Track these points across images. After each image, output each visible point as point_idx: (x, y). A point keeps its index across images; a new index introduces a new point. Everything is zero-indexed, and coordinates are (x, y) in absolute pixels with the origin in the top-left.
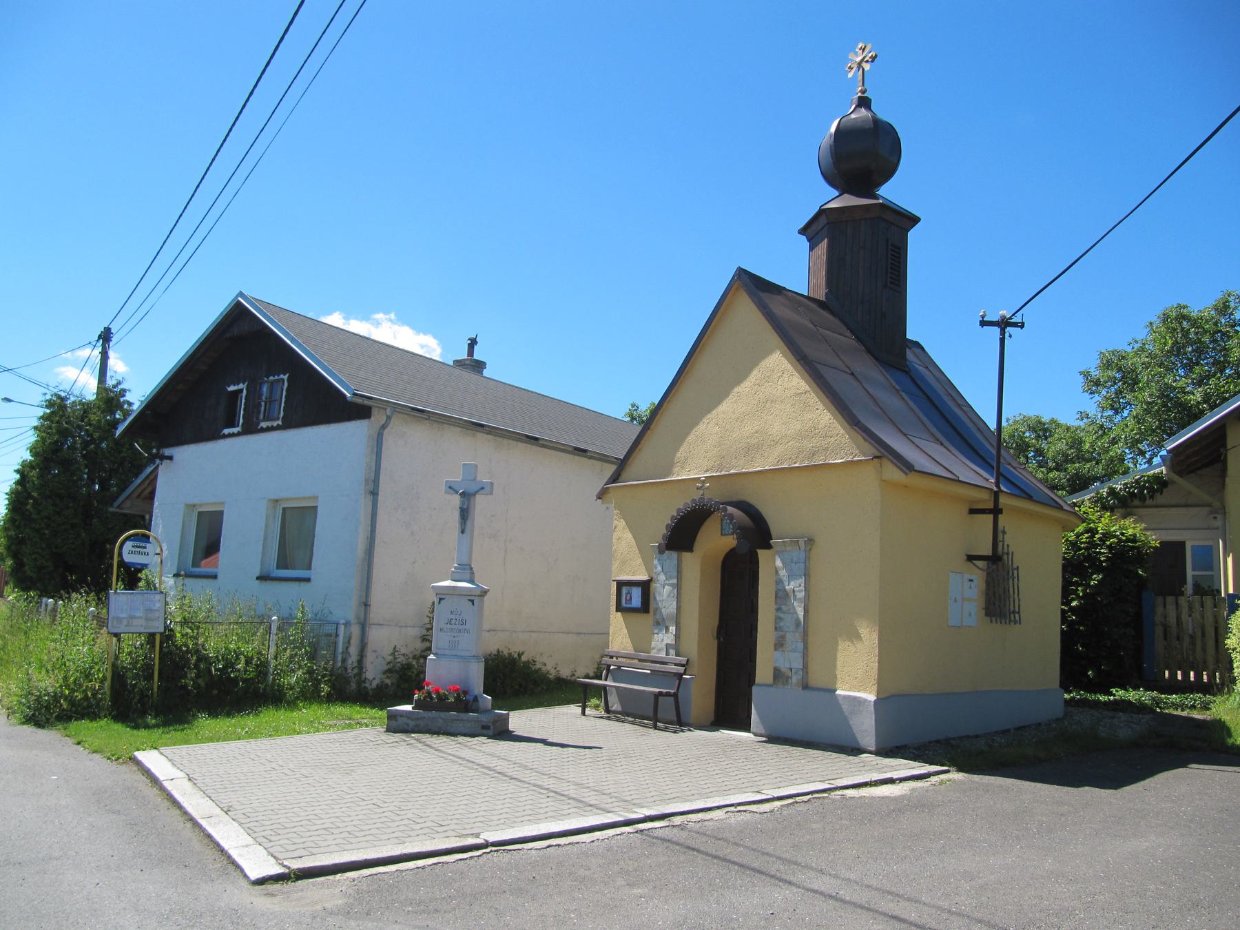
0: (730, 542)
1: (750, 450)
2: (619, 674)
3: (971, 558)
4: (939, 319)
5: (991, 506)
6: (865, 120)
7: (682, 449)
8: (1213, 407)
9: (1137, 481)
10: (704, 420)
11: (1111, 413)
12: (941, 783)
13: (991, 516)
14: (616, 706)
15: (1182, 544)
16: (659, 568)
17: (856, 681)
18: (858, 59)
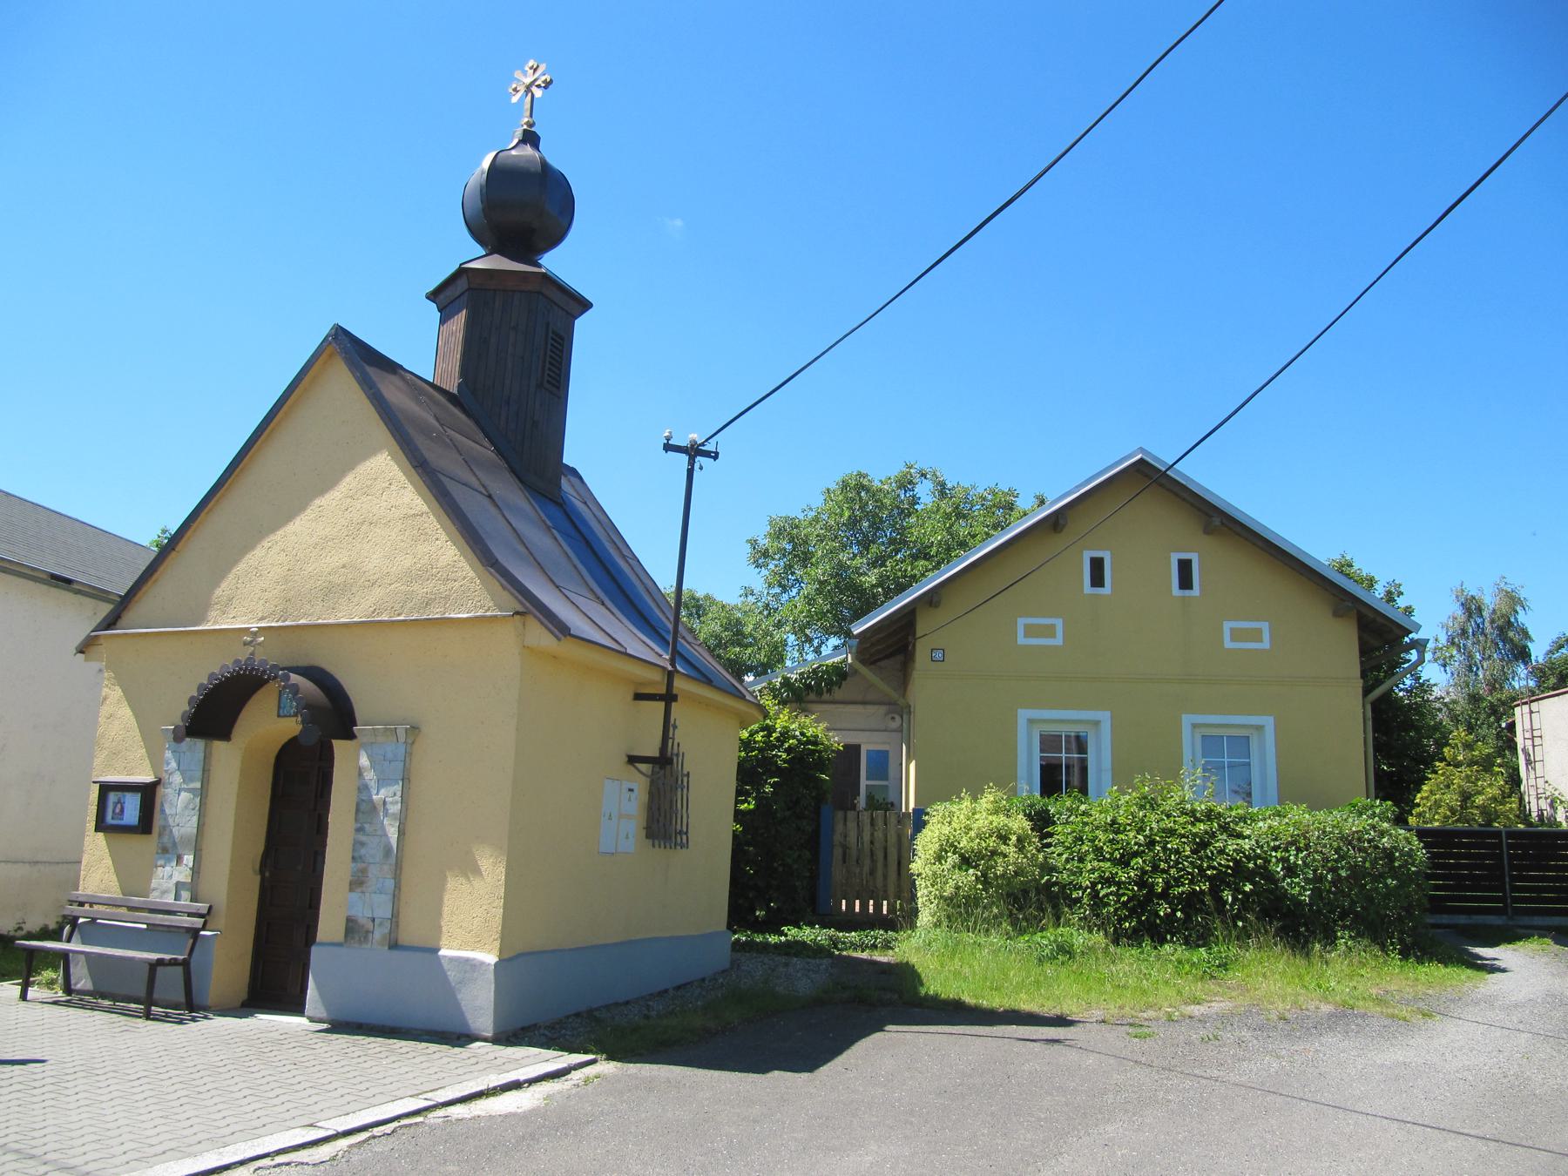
0: (292, 727)
1: (332, 592)
2: (94, 931)
3: (633, 760)
4: (609, 438)
5: (663, 690)
6: (529, 160)
7: (224, 585)
8: (889, 595)
9: (815, 671)
10: (266, 543)
11: (778, 590)
12: (587, 1081)
13: (661, 705)
14: (82, 981)
15: (857, 748)
16: (174, 765)
17: (470, 935)
18: (528, 81)
